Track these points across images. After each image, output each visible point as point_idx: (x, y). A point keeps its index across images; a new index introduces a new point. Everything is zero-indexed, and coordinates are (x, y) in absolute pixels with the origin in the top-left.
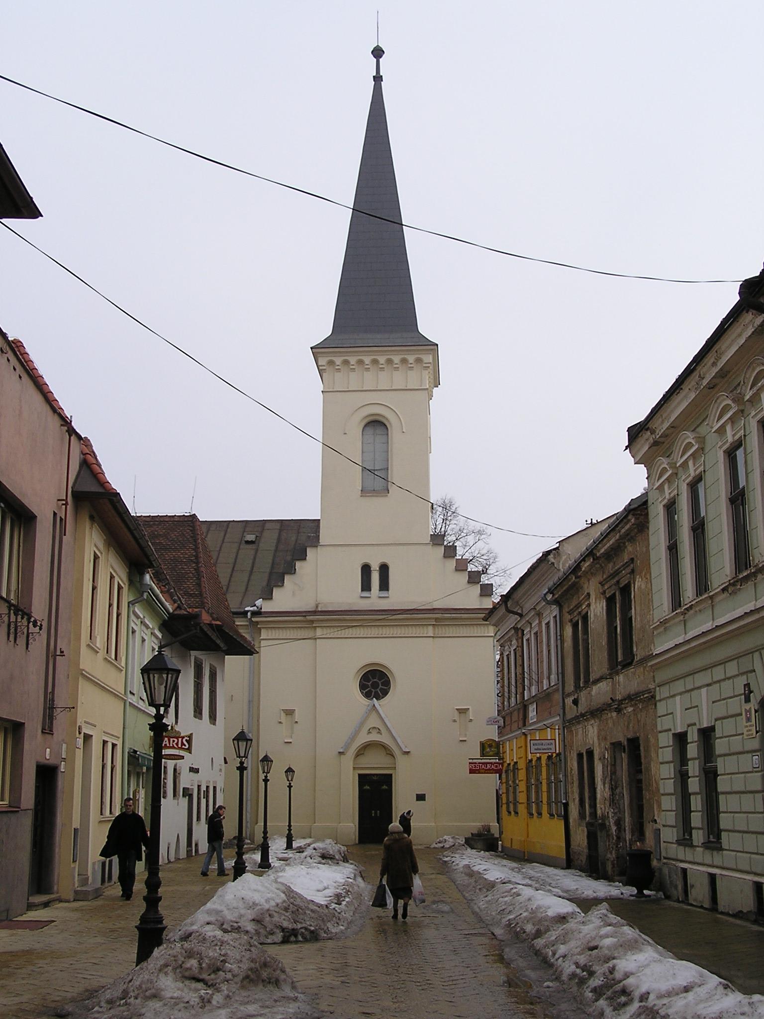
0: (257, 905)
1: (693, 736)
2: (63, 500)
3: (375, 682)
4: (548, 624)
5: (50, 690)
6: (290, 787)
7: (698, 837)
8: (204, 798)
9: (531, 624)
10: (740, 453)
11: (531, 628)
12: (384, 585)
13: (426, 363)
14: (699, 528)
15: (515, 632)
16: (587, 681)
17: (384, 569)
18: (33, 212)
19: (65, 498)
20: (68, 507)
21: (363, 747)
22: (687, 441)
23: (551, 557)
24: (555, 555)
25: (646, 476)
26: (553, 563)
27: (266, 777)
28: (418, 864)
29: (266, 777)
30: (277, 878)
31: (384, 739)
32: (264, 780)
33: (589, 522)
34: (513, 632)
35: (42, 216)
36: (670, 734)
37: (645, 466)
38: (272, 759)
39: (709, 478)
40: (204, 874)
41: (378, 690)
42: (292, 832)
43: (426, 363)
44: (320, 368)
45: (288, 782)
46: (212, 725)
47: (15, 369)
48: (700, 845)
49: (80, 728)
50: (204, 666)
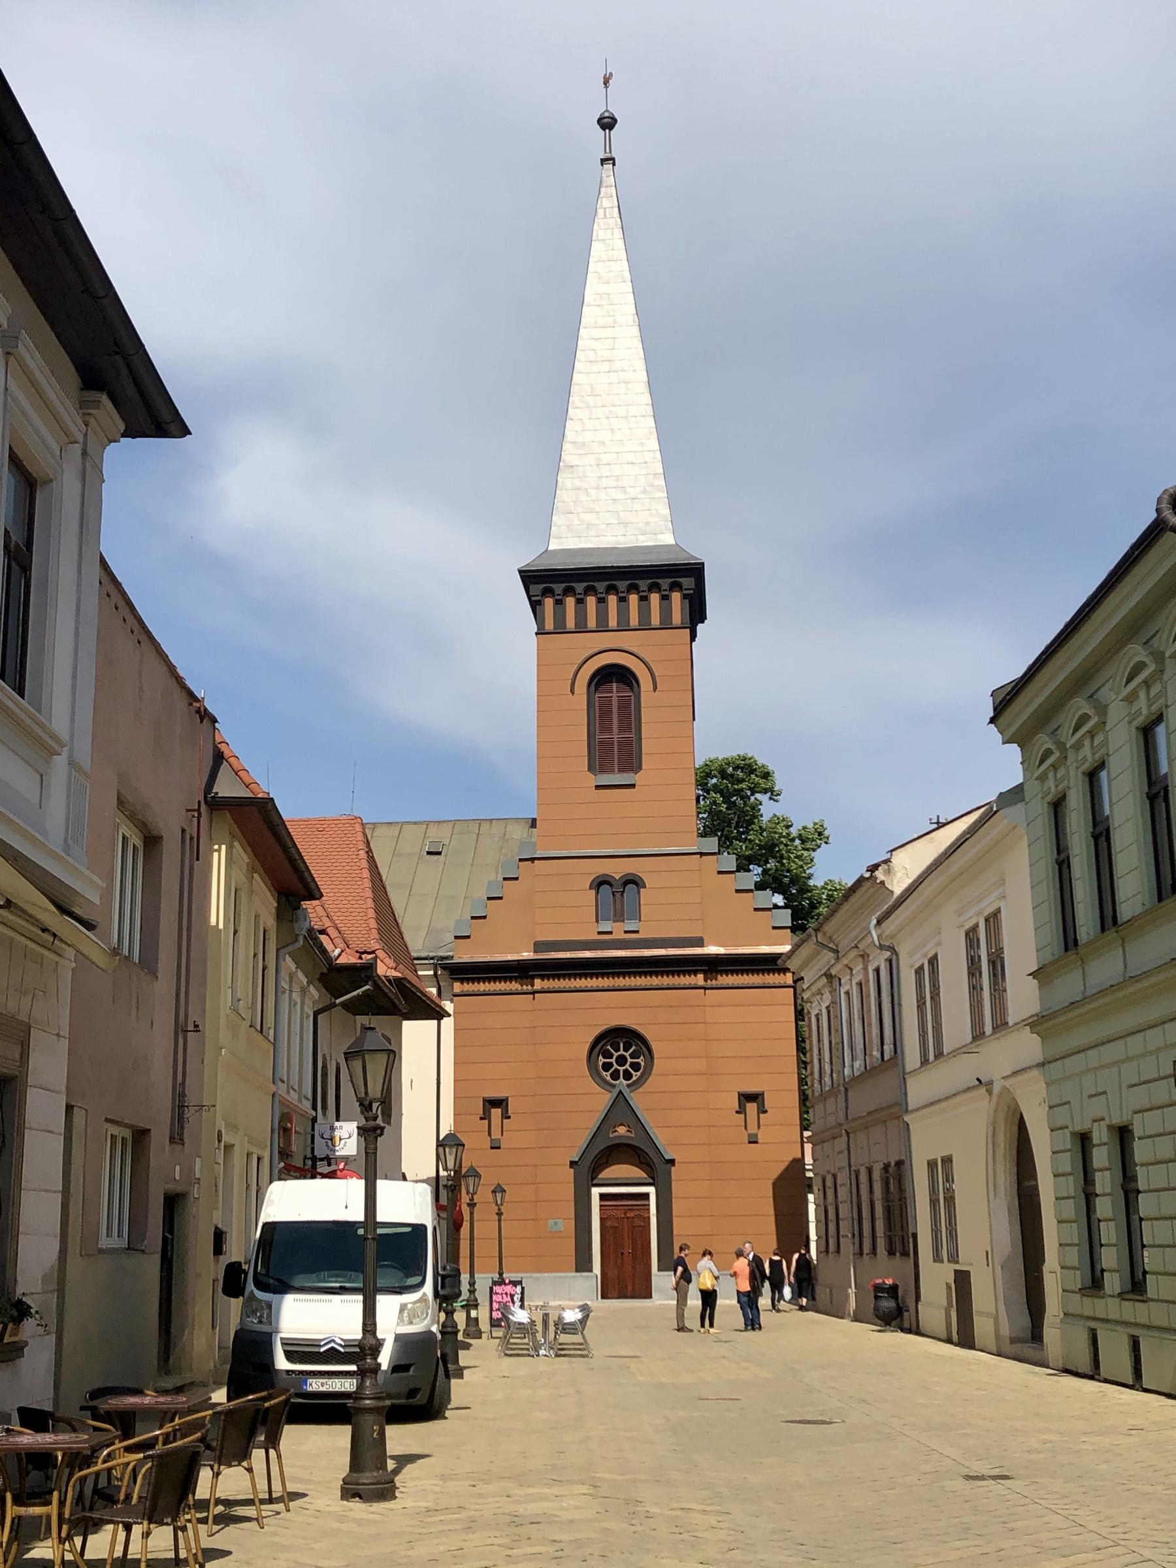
1: (1100, 1135)
2: (194, 810)
3: (626, 1059)
4: (877, 970)
5: (180, 1080)
6: (500, 1214)
7: (1113, 1283)
9: (851, 969)
10: (1161, 730)
11: (852, 975)
13: (686, 589)
14: (1101, 835)
15: (828, 982)
16: (939, 1054)
18: (185, 431)
19: (197, 808)
22: (1080, 713)
23: (880, 875)
24: (884, 871)
25: (1021, 760)
26: (883, 883)
27: (472, 1199)
28: (155, 1353)
29: (472, 1199)
32: (469, 1205)
34: (824, 980)
35: (190, 434)
36: (1067, 1132)
37: (1019, 746)
39: (1114, 764)
40: (681, 1329)
43: (686, 589)
44: (533, 598)
45: (497, 1207)
47: (132, 632)
48: (1077, 1290)
49: (220, 1134)
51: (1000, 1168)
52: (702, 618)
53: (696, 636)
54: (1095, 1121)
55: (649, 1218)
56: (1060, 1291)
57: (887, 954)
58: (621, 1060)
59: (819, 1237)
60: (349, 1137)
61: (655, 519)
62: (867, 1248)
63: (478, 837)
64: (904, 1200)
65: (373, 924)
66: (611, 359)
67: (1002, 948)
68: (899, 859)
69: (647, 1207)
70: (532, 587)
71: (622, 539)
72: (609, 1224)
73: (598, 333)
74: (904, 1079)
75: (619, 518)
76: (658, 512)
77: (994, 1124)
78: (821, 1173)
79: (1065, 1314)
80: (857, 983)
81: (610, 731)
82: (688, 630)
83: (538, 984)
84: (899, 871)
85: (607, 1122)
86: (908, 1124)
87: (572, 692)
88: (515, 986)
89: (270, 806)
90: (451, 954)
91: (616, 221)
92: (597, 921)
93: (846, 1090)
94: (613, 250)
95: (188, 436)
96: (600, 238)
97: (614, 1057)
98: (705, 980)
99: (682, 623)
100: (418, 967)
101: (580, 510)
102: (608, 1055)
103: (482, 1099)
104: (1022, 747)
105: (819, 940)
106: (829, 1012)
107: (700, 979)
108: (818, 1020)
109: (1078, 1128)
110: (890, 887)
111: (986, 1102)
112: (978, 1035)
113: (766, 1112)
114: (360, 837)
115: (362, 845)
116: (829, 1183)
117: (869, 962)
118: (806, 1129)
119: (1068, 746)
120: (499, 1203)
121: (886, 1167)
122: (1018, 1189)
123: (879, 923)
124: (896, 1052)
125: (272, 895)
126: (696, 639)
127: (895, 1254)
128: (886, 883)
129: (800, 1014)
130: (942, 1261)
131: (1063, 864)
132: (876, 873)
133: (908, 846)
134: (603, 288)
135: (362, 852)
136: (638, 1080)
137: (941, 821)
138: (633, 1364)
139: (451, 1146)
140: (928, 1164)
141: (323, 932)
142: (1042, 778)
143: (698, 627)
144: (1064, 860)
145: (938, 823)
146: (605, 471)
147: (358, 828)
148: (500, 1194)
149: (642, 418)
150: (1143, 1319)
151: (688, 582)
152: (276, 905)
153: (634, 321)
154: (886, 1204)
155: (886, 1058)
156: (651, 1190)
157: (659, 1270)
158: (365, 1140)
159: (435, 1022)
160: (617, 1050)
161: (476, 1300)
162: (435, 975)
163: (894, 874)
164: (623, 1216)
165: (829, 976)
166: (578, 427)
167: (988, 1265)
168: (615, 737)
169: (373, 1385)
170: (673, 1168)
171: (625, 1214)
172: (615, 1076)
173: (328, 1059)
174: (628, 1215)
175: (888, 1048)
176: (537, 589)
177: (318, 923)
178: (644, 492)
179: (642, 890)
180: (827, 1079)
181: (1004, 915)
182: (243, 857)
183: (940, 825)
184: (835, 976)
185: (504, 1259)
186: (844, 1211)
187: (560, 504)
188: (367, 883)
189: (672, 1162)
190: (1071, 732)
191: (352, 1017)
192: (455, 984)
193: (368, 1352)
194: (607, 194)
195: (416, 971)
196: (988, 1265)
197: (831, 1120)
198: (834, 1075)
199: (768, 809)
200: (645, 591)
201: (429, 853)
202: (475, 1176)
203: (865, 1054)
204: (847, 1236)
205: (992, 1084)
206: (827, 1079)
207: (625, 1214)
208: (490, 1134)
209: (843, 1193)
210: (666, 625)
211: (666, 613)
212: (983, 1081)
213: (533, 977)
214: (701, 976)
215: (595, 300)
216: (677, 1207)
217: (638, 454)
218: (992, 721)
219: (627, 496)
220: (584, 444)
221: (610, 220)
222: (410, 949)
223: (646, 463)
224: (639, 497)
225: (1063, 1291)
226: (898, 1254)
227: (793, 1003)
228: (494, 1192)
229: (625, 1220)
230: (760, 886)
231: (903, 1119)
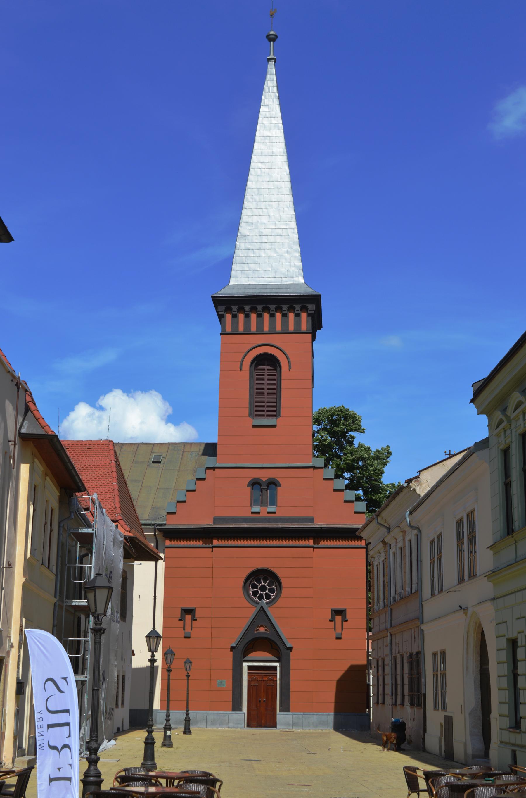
0: (360, 426)
4: (410, 541)
6: (188, 676)
11: (396, 542)
13: (310, 310)
16: (441, 591)
20: (17, 446)
23: (413, 485)
26: (414, 490)
33: (448, 453)
36: (505, 638)
37: (487, 416)
38: (175, 653)
42: (189, 715)
43: (310, 310)
44: (220, 313)
52: (320, 327)
53: (315, 337)
54: (519, 633)
55: (276, 681)
56: (499, 729)
58: (263, 588)
59: (374, 695)
61: (293, 268)
62: (399, 702)
63: (183, 453)
64: (420, 674)
65: (118, 504)
66: (270, 174)
67: (475, 531)
69: (275, 675)
70: (219, 307)
71: (273, 279)
72: (253, 683)
73: (263, 159)
74: (422, 604)
75: (272, 267)
76: (295, 265)
77: (468, 632)
78: (376, 657)
79: (500, 742)
80: (399, 548)
81: (263, 392)
82: (311, 334)
83: (215, 542)
84: (424, 484)
85: (253, 625)
86: (423, 631)
87: (241, 369)
88: (200, 543)
89: (55, 439)
90: (165, 522)
91: (275, 94)
92: (251, 506)
94: (273, 111)
95: (12, 241)
96: (266, 104)
97: (259, 587)
99: (307, 331)
100: (144, 530)
101: (249, 262)
102: (255, 586)
103: (180, 608)
104: (489, 416)
105: (379, 522)
106: (384, 564)
107: (311, 542)
108: (378, 568)
109: (511, 636)
112: (461, 581)
113: (347, 621)
114: (112, 452)
115: (113, 458)
116: (380, 663)
117: (406, 535)
118: (371, 631)
119: (511, 418)
121: (411, 655)
122: (480, 670)
123: (411, 513)
124: (418, 589)
125: (57, 489)
126: (316, 339)
127: (414, 705)
129: (368, 563)
130: (438, 710)
131: (507, 486)
132: (411, 484)
134: (267, 133)
135: (113, 462)
136: (275, 598)
137: (451, 453)
138: (255, 764)
139: (153, 637)
140: (433, 654)
141: (87, 509)
142: (498, 436)
143: (317, 332)
144: (509, 483)
145: (449, 454)
146: (265, 239)
147: (111, 447)
149: (287, 209)
150: (519, 742)
151: (311, 307)
152: (59, 494)
153: (284, 153)
154: (409, 676)
155: (413, 591)
156: (277, 664)
157: (280, 711)
158: (95, 635)
159: (154, 563)
160: (260, 583)
161: (170, 725)
162: (155, 535)
164: (261, 679)
165: (384, 542)
166: (250, 214)
167: (462, 713)
168: (266, 396)
169: (95, 769)
170: (291, 653)
171: (262, 678)
172: (261, 597)
174: (264, 679)
175: (414, 586)
176: (222, 308)
177: (84, 504)
178: (287, 252)
179: (278, 488)
180: (381, 603)
181: (476, 513)
182: (40, 467)
183: (451, 456)
185: (171, 703)
186: (388, 680)
187: (237, 258)
188: (115, 480)
189: (290, 649)
190: (513, 412)
192: (166, 541)
193: (93, 751)
194: (270, 78)
195: (143, 533)
196: (462, 713)
197: (382, 627)
198: (385, 601)
199: (358, 439)
200: (286, 311)
201: (154, 462)
203: (402, 589)
204: (388, 694)
205: (467, 609)
206: (381, 603)
207: (262, 678)
208: (184, 629)
209: (388, 669)
210: (298, 332)
211: (298, 324)
212: (463, 608)
213: (212, 538)
215: (261, 140)
216: (293, 675)
217: (283, 230)
218: (472, 401)
219: (277, 254)
220: (252, 223)
221: (272, 94)
222: (140, 519)
223: (289, 235)
224: (284, 255)
225: (500, 729)
227: (365, 557)
228: (185, 663)
229: (262, 681)
230: (347, 487)
231: (420, 628)
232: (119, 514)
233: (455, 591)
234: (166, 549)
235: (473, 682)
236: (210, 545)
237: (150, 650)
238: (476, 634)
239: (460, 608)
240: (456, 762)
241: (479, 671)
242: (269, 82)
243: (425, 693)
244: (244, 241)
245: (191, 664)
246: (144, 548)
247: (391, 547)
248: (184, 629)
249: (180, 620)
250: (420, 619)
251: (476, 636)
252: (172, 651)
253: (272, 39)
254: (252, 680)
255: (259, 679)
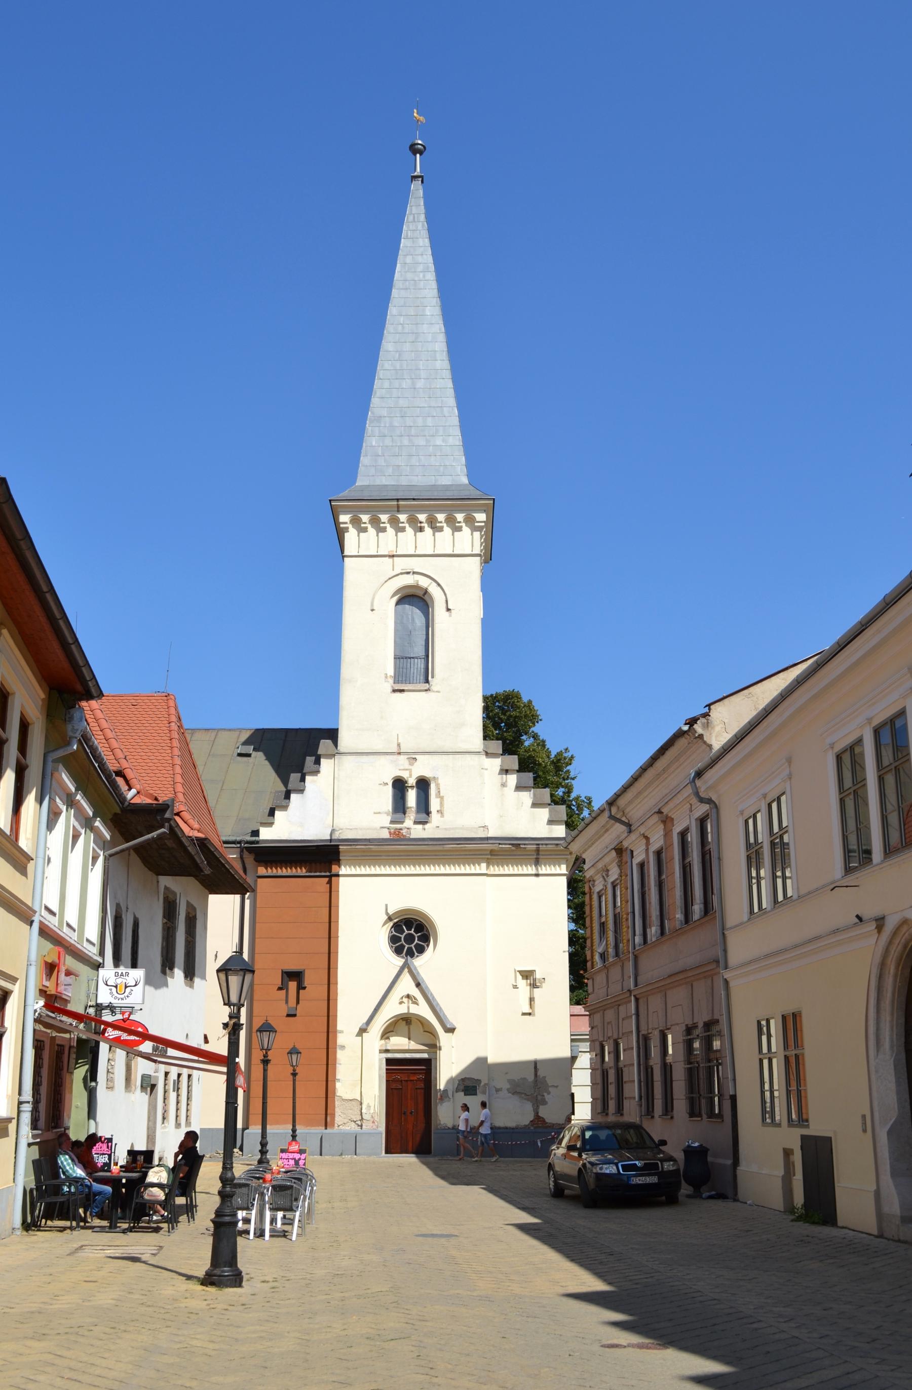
6: (294, 1074)
8: (174, 1091)
12: (424, 807)
17: (423, 785)
21: (393, 1022)
23: (698, 728)
24: (703, 724)
26: (701, 736)
30: (112, 1060)
31: (422, 1010)
36: (658, 1030)
38: (277, 1029)
41: (413, 946)
46: (188, 988)
50: (178, 901)
51: (886, 1017)
57: (703, 808)
60: (136, 985)
68: (718, 712)
77: (883, 965)
84: (718, 725)
93: (636, 958)
98: (488, 867)
110: (708, 742)
111: (873, 940)
120: (294, 1064)
122: (905, 1043)
128: (705, 737)
132: (695, 726)
133: (726, 701)
139: (236, 972)
148: (296, 1056)
153: (437, 302)
163: (713, 728)
164: (406, 1079)
167: (865, 1131)
173: (124, 909)
184: (627, 848)
191: (155, 876)
196: (865, 1131)
202: (270, 1031)
208: (287, 1002)
214: (484, 865)
226: (704, 1116)
228: (290, 1053)
232: (180, 803)
233: (847, 886)
234: (258, 879)
235: (892, 1066)
236: (328, 874)
237: (228, 1003)
238: (900, 968)
239: (858, 921)
240: (843, 1228)
241: (903, 1045)
242: (414, 208)
243: (733, 1093)
244: (378, 425)
245: (299, 1055)
246: (223, 865)
247: (634, 854)
248: (287, 1002)
249: (280, 989)
250: (720, 962)
251: (899, 973)
252: (270, 1025)
253: (414, 150)
254: (395, 1081)
255: (403, 1079)
